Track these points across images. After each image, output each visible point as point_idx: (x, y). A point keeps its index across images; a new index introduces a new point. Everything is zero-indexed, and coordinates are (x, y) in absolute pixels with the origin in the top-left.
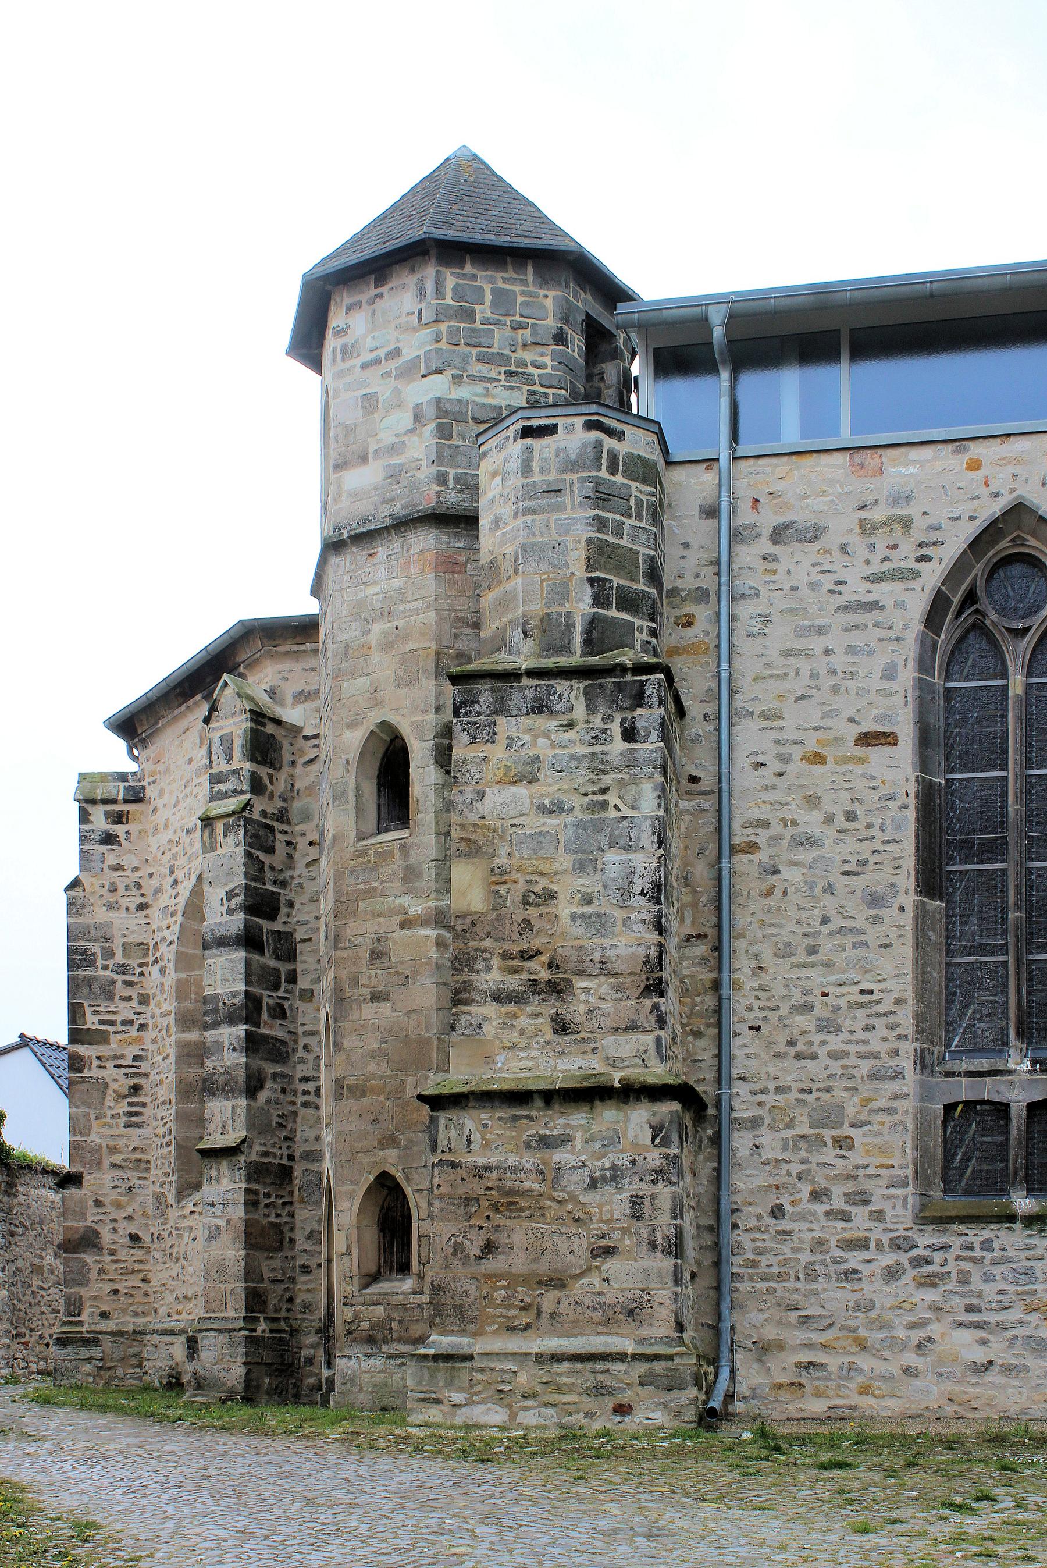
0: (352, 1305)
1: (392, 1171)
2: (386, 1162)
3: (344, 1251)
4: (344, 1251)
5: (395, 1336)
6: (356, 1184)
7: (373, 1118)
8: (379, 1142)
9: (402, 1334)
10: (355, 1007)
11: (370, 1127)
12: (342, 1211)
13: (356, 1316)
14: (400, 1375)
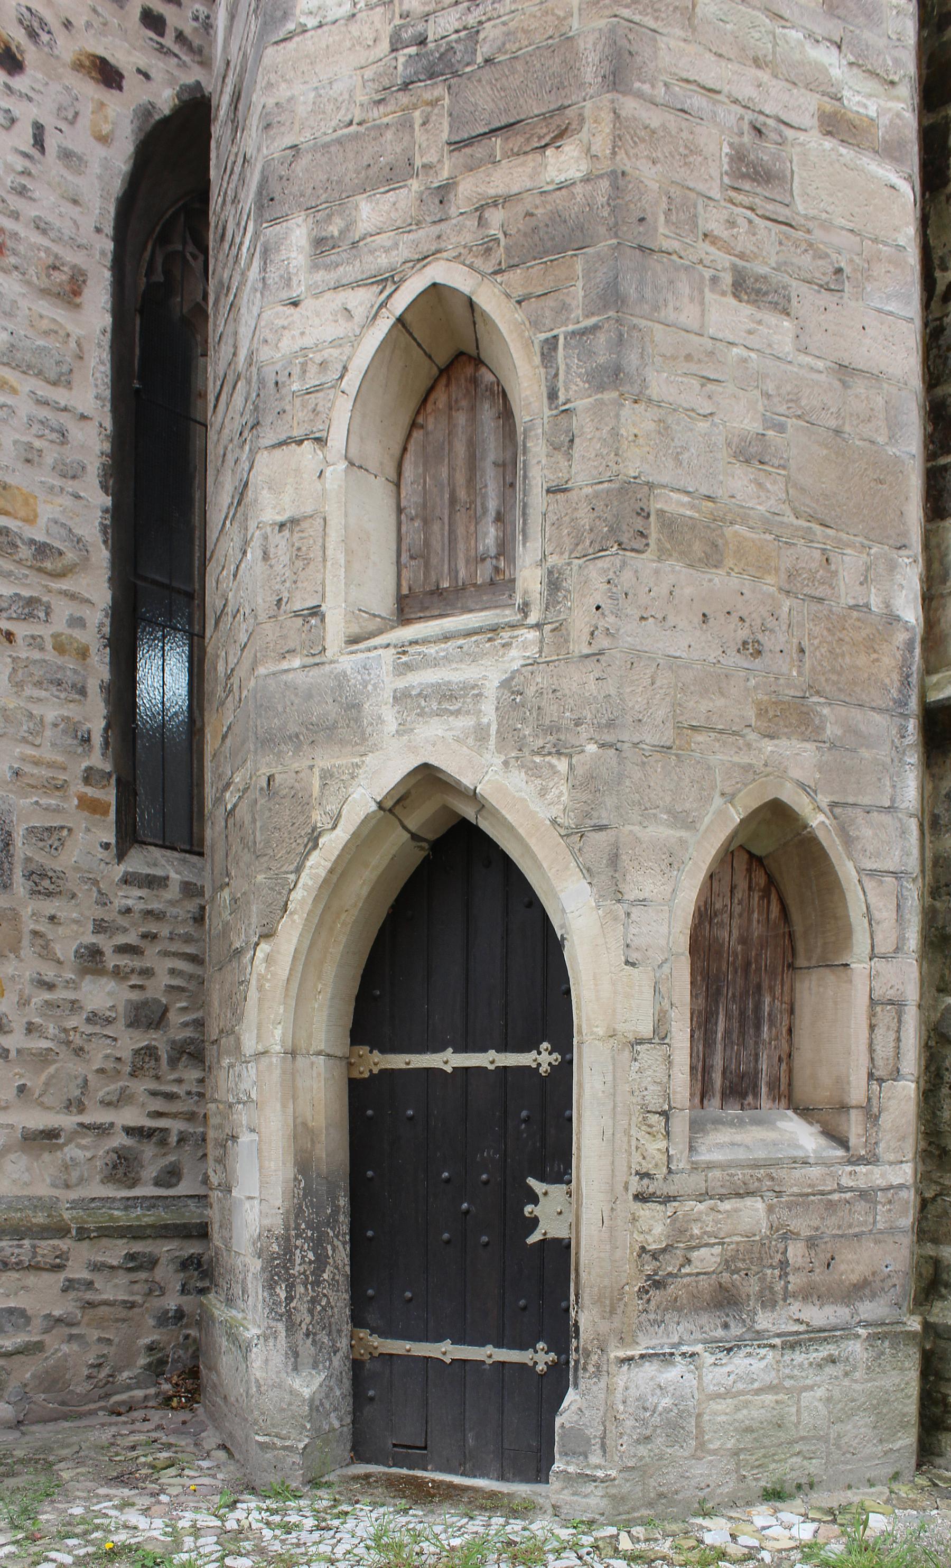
0: (668, 1199)
1: (801, 804)
2: (783, 774)
3: (646, 1029)
4: (646, 1029)
5: (796, 1281)
6: (691, 825)
7: (743, 634)
8: (762, 712)
9: (816, 1277)
10: (684, 288)
11: (733, 659)
12: (643, 902)
13: (679, 1230)
14: (820, 1392)
